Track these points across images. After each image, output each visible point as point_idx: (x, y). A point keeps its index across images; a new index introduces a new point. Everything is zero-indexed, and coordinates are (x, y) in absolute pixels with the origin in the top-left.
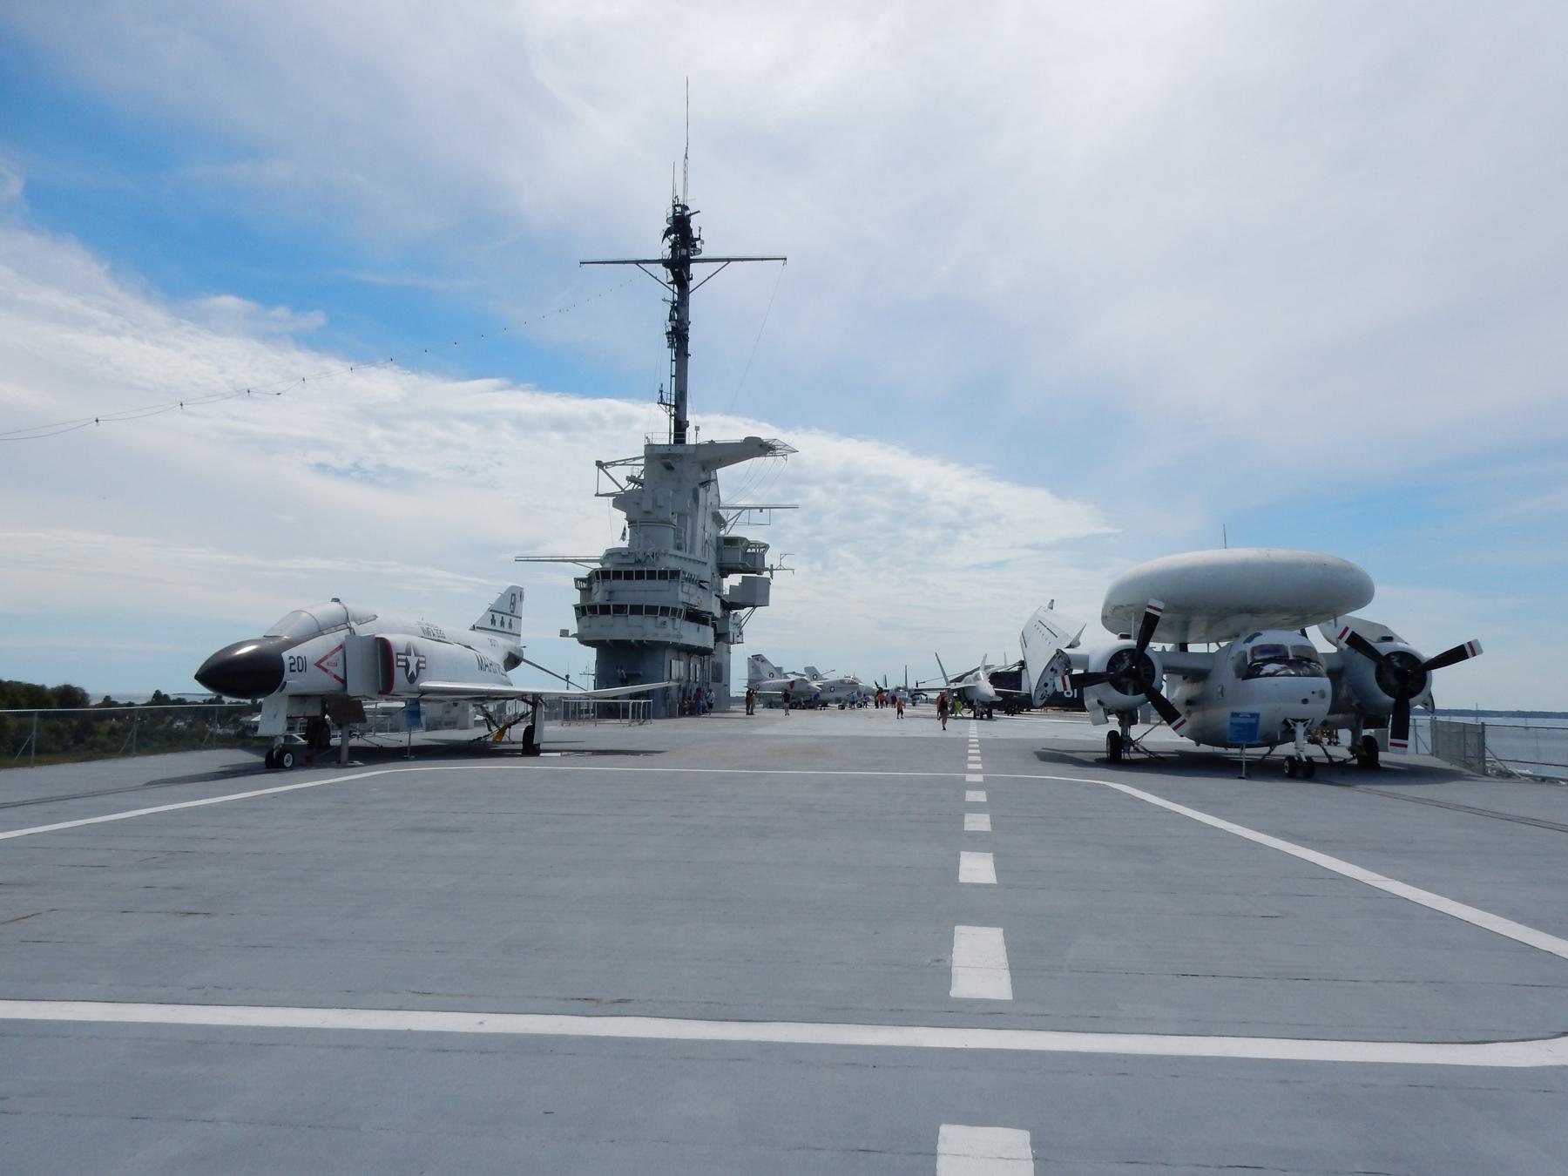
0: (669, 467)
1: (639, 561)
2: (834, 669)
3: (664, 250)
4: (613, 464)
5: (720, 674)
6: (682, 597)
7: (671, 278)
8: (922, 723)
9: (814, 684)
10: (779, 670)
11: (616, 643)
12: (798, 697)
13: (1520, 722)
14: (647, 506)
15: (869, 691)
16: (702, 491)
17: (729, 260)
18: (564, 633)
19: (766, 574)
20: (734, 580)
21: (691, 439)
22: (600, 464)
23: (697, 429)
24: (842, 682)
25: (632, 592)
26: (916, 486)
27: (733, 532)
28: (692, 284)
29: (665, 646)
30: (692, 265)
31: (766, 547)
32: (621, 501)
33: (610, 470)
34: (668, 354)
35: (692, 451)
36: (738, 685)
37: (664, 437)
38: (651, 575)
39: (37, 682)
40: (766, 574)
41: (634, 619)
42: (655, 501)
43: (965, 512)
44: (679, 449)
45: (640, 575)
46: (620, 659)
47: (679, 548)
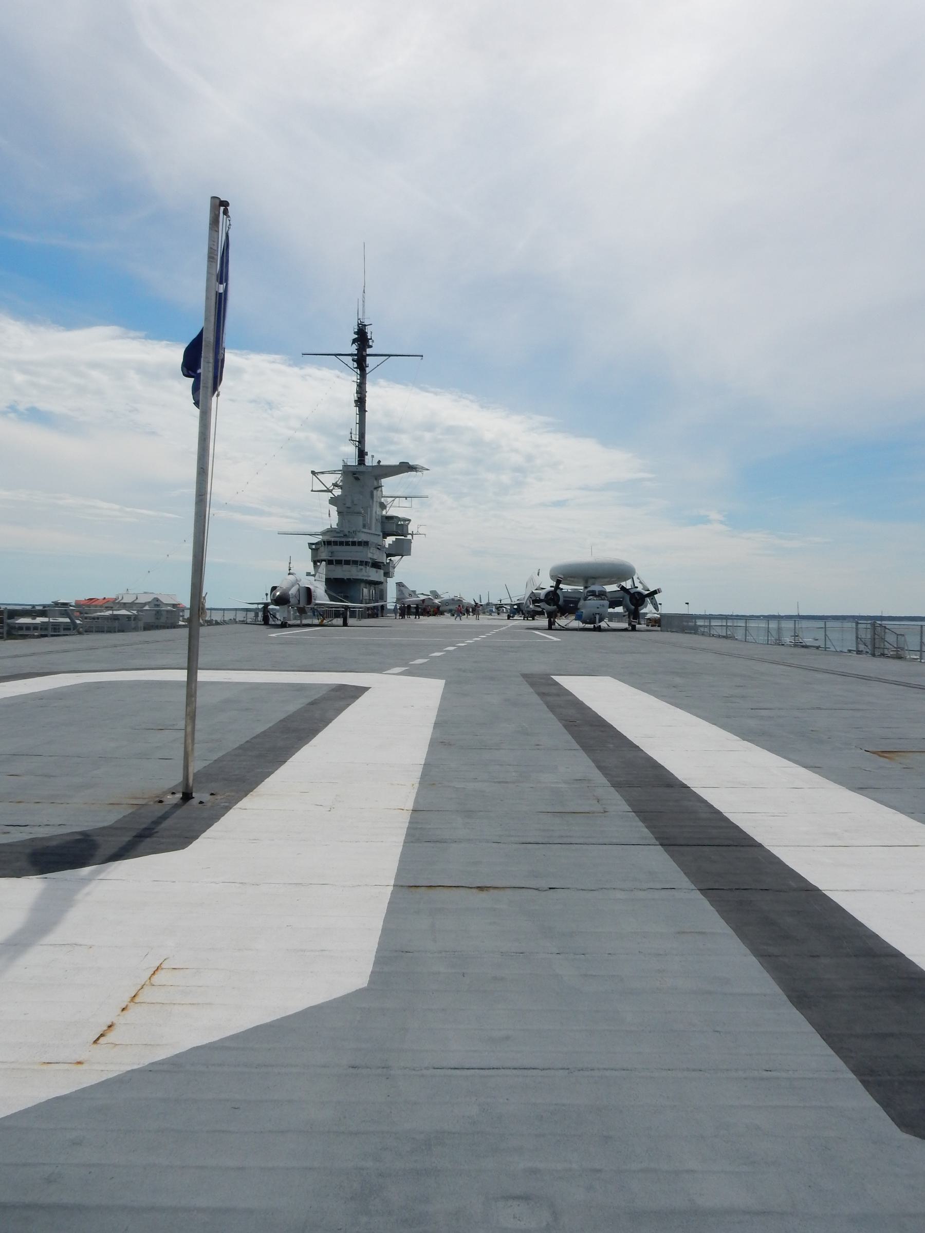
0: (357, 479)
1: (345, 535)
2: (447, 592)
3: (353, 349)
4: (322, 473)
5: (382, 596)
6: (370, 555)
7: (356, 365)
8: (501, 621)
9: (437, 601)
10: (414, 592)
11: (336, 579)
12: (426, 608)
14: (349, 504)
16: (375, 492)
17: (390, 356)
18: (308, 574)
19: (409, 537)
20: (390, 540)
21: (368, 461)
22: (313, 473)
23: (373, 456)
24: (453, 600)
25: (344, 553)
26: (488, 436)
27: (391, 512)
28: (368, 370)
29: (362, 581)
30: (368, 358)
31: (409, 520)
32: (333, 501)
33: (320, 476)
34: (355, 410)
35: (370, 470)
37: (353, 461)
38: (354, 543)
40: (409, 537)
41: (346, 567)
42: (353, 502)
43: (529, 458)
44: (362, 468)
45: (347, 544)
46: (335, 586)
47: (364, 526)
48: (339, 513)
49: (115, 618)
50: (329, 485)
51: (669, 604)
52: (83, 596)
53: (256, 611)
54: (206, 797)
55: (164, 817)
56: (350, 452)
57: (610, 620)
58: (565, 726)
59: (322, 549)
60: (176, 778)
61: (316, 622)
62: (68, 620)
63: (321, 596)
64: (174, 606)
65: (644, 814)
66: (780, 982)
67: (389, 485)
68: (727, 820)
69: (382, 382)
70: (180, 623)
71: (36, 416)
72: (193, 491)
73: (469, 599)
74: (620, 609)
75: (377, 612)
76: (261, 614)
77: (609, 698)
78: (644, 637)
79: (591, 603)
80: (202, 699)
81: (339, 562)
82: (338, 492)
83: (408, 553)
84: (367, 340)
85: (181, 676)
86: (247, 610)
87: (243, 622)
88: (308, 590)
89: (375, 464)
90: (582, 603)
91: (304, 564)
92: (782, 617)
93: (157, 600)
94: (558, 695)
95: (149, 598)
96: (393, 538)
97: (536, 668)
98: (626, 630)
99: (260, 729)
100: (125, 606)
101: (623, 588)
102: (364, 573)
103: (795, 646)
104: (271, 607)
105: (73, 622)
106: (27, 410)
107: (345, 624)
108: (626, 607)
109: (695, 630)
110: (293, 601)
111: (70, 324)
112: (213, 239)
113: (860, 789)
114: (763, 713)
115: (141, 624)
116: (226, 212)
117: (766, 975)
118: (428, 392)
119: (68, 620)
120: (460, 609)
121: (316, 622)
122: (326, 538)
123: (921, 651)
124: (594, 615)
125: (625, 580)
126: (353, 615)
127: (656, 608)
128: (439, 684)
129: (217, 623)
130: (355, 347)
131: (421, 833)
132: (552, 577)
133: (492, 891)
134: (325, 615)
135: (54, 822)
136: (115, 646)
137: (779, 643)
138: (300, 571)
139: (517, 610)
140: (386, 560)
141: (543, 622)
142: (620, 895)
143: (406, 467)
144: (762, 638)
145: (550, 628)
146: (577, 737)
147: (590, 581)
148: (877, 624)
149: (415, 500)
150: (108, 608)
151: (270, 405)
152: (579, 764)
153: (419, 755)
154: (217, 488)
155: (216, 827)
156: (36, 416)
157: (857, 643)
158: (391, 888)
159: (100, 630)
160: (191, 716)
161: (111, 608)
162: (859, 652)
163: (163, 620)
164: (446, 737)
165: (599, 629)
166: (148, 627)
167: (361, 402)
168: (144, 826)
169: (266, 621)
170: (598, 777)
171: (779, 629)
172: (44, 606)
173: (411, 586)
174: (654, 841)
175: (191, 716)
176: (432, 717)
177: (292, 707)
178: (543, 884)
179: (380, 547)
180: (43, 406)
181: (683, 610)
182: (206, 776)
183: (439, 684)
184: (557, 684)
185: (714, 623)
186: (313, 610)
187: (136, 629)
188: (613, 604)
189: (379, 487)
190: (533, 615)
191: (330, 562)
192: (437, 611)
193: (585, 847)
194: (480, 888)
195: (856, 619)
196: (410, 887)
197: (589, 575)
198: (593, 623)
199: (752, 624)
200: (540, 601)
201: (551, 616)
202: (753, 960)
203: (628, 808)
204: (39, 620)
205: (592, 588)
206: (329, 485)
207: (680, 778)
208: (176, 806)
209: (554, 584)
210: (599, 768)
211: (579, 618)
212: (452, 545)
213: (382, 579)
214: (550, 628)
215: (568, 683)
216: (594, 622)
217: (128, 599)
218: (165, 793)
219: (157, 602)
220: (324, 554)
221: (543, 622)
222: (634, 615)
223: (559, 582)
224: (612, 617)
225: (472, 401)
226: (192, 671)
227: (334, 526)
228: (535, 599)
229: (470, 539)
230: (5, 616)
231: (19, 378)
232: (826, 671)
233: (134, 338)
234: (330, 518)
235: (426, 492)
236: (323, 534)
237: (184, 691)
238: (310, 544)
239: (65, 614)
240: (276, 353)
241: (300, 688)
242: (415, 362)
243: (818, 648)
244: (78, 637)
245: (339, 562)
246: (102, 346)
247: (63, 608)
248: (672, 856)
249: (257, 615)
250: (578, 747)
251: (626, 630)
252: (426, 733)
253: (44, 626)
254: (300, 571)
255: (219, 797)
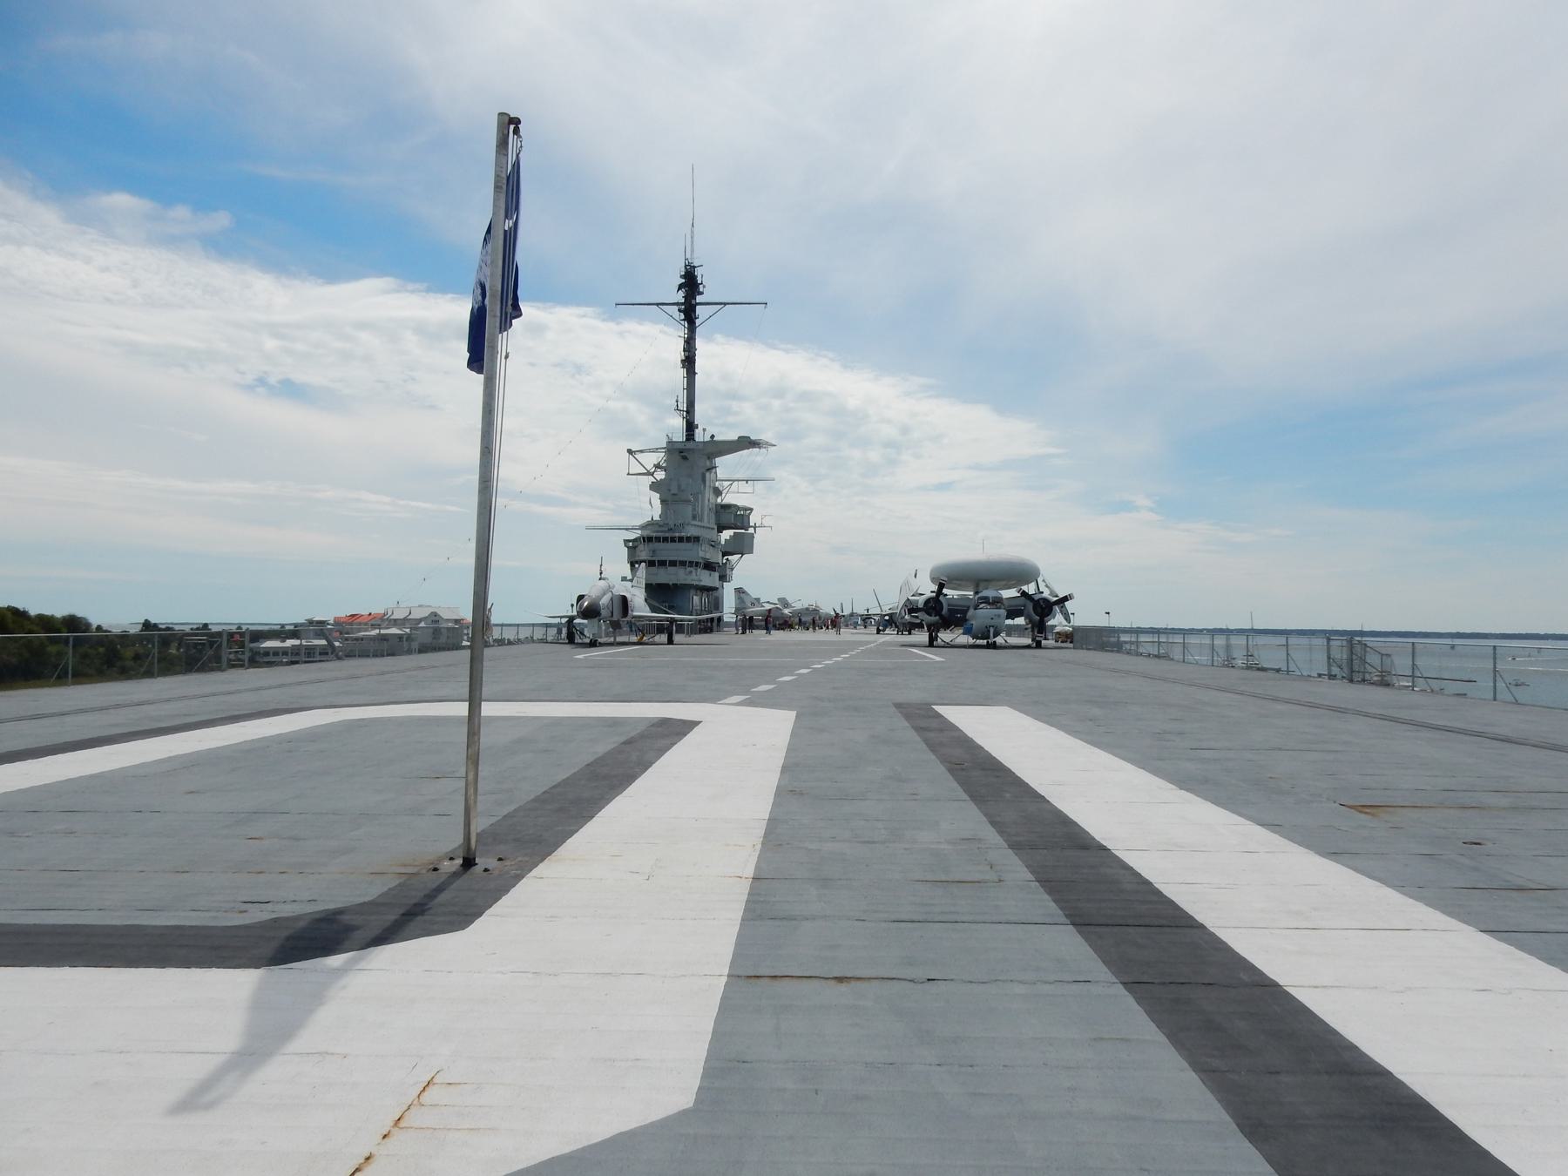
0: (685, 458)
2: (800, 599)
3: (680, 297)
5: (717, 605)
6: (701, 554)
8: (869, 636)
9: (786, 611)
11: (659, 585)
12: (775, 621)
13: (1449, 641)
15: (828, 616)
18: (624, 579)
19: (751, 530)
20: (726, 535)
21: (699, 436)
22: (630, 451)
26: (852, 403)
27: (728, 499)
28: (698, 322)
29: (690, 587)
32: (654, 487)
34: (682, 372)
36: (728, 612)
37: (679, 436)
38: (681, 539)
39: (47, 612)
41: (671, 569)
43: (905, 430)
44: (690, 445)
45: (673, 540)
46: (658, 593)
47: (694, 518)
48: (663, 501)
49: (384, 638)
50: (650, 467)
51: (1084, 613)
52: (344, 612)
53: (559, 627)
54: (491, 863)
55: (440, 889)
56: (677, 423)
57: (1009, 635)
58: (950, 771)
59: (641, 547)
60: (453, 840)
61: (634, 639)
62: (324, 642)
63: (640, 606)
64: (457, 621)
65: (1050, 883)
66: (1228, 1105)
67: (725, 465)
68: (1158, 893)
69: (719, 337)
70: (461, 642)
71: (291, 390)
72: (476, 477)
73: (827, 609)
74: (1020, 621)
75: (711, 626)
76: (564, 631)
77: (1006, 733)
78: (1053, 656)
79: (983, 612)
80: (486, 738)
81: (662, 563)
82: (660, 475)
83: (751, 552)
84: (697, 285)
85: (462, 709)
86: (547, 626)
87: (543, 641)
88: (624, 599)
89: (707, 438)
90: (971, 612)
91: (619, 566)
92: (1231, 631)
93: (435, 614)
94: (941, 730)
95: (425, 613)
96: (731, 532)
97: (914, 696)
98: (1028, 647)
99: (562, 776)
100: (395, 623)
101: (1024, 594)
102: (693, 576)
103: (1249, 668)
104: (577, 621)
105: (330, 644)
106: (280, 382)
107: (670, 642)
108: (1028, 617)
109: (1118, 647)
110: (604, 613)
111: (331, 275)
112: (499, 165)
113: (1333, 854)
114: (1207, 754)
115: (415, 645)
116: (516, 131)
117: (1210, 1097)
118: (775, 348)
119: (324, 642)
120: (811, 620)
121: (634, 639)
122: (647, 533)
123: (1413, 676)
124: (987, 628)
125: (1028, 583)
126: (680, 629)
127: (1068, 619)
128: (791, 715)
129: (510, 643)
130: (682, 293)
131: (762, 907)
132: (933, 580)
133: (853, 983)
134: (644, 631)
135: (301, 897)
136: (383, 674)
137: (1229, 664)
138: (615, 575)
139: (889, 622)
140: (719, 559)
141: (922, 637)
142: (1020, 989)
143: (746, 443)
144: (1205, 659)
145: (931, 645)
146: (966, 785)
147: (982, 585)
148: (1354, 640)
149: (759, 485)
150: (374, 626)
151: (579, 369)
152: (968, 819)
153: (759, 807)
154: (506, 472)
155: (505, 901)
156: (291, 390)
157: (1329, 665)
158: (724, 979)
159: (364, 654)
160: (473, 760)
161: (379, 627)
162: (1332, 677)
163: (443, 640)
164: (797, 784)
165: (994, 646)
166: (423, 650)
167: (689, 362)
168: (414, 901)
169: (571, 639)
170: (991, 836)
171: (1228, 647)
172: (296, 625)
173: (753, 592)
174: (1064, 920)
175: (473, 760)
176: (779, 759)
177: (602, 749)
178: (921, 973)
179: (714, 544)
180: (299, 377)
181: (1102, 622)
182: (493, 836)
183: (791, 715)
184: (939, 716)
185: (1143, 638)
186: (630, 624)
187: (409, 652)
188: (1012, 614)
189: (712, 468)
190: (910, 628)
191: (651, 564)
192: (786, 625)
193: (974, 926)
194: (840, 979)
195: (1328, 635)
196: (748, 976)
197: (980, 577)
198: (986, 639)
199: (1192, 640)
200: (917, 610)
201: (933, 630)
202: (1192, 1077)
203: (1030, 876)
204: (290, 643)
205: (985, 593)
206: (650, 467)
207: (1097, 837)
208: (455, 875)
209: (935, 588)
210: (993, 823)
211: (967, 632)
212: (812, 540)
213: (717, 583)
214: (931, 645)
215: (956, 715)
216: (987, 637)
217: (399, 615)
218: (440, 860)
219: (434, 618)
220: (644, 554)
221: (922, 637)
222: (1039, 627)
223: (941, 586)
224: (1011, 630)
225: (832, 360)
226: (474, 702)
227: (657, 518)
228: (912, 608)
229: (838, 524)
230: (247, 639)
231: (271, 344)
232: (1287, 701)
233: (413, 292)
234: (649, 508)
235: (773, 474)
236: (642, 527)
237: (465, 729)
238: (626, 541)
239: (320, 634)
240: (588, 305)
241: (614, 723)
242: (761, 314)
243: (1278, 670)
244: (338, 664)
245: (662, 563)
246: (373, 301)
247: (318, 627)
248: (1087, 940)
249: (559, 632)
250: (965, 797)
251: (1028, 647)
252: (770, 780)
253: (295, 651)
254: (615, 575)
255: (508, 863)
